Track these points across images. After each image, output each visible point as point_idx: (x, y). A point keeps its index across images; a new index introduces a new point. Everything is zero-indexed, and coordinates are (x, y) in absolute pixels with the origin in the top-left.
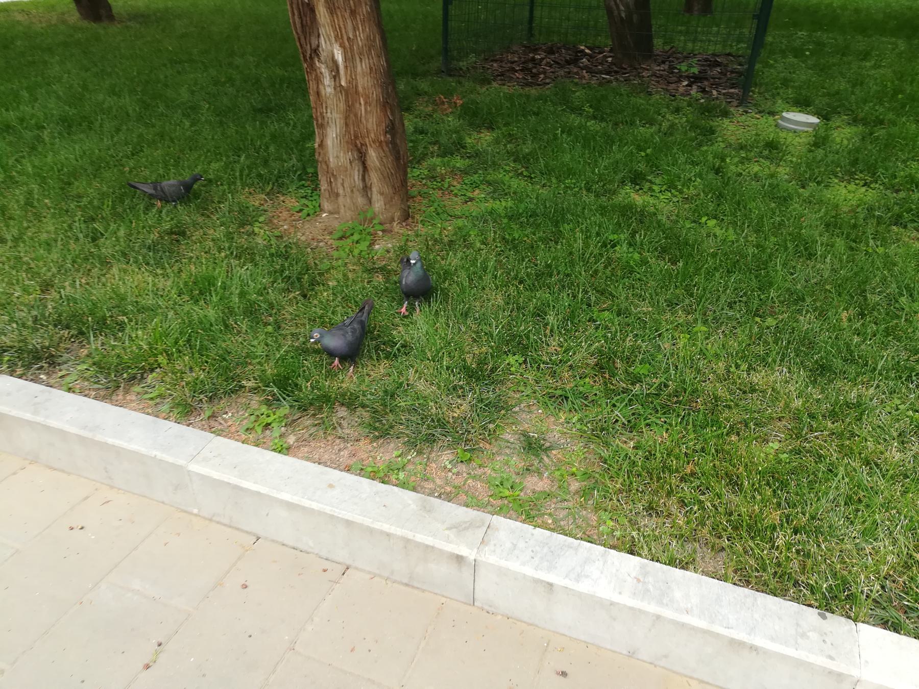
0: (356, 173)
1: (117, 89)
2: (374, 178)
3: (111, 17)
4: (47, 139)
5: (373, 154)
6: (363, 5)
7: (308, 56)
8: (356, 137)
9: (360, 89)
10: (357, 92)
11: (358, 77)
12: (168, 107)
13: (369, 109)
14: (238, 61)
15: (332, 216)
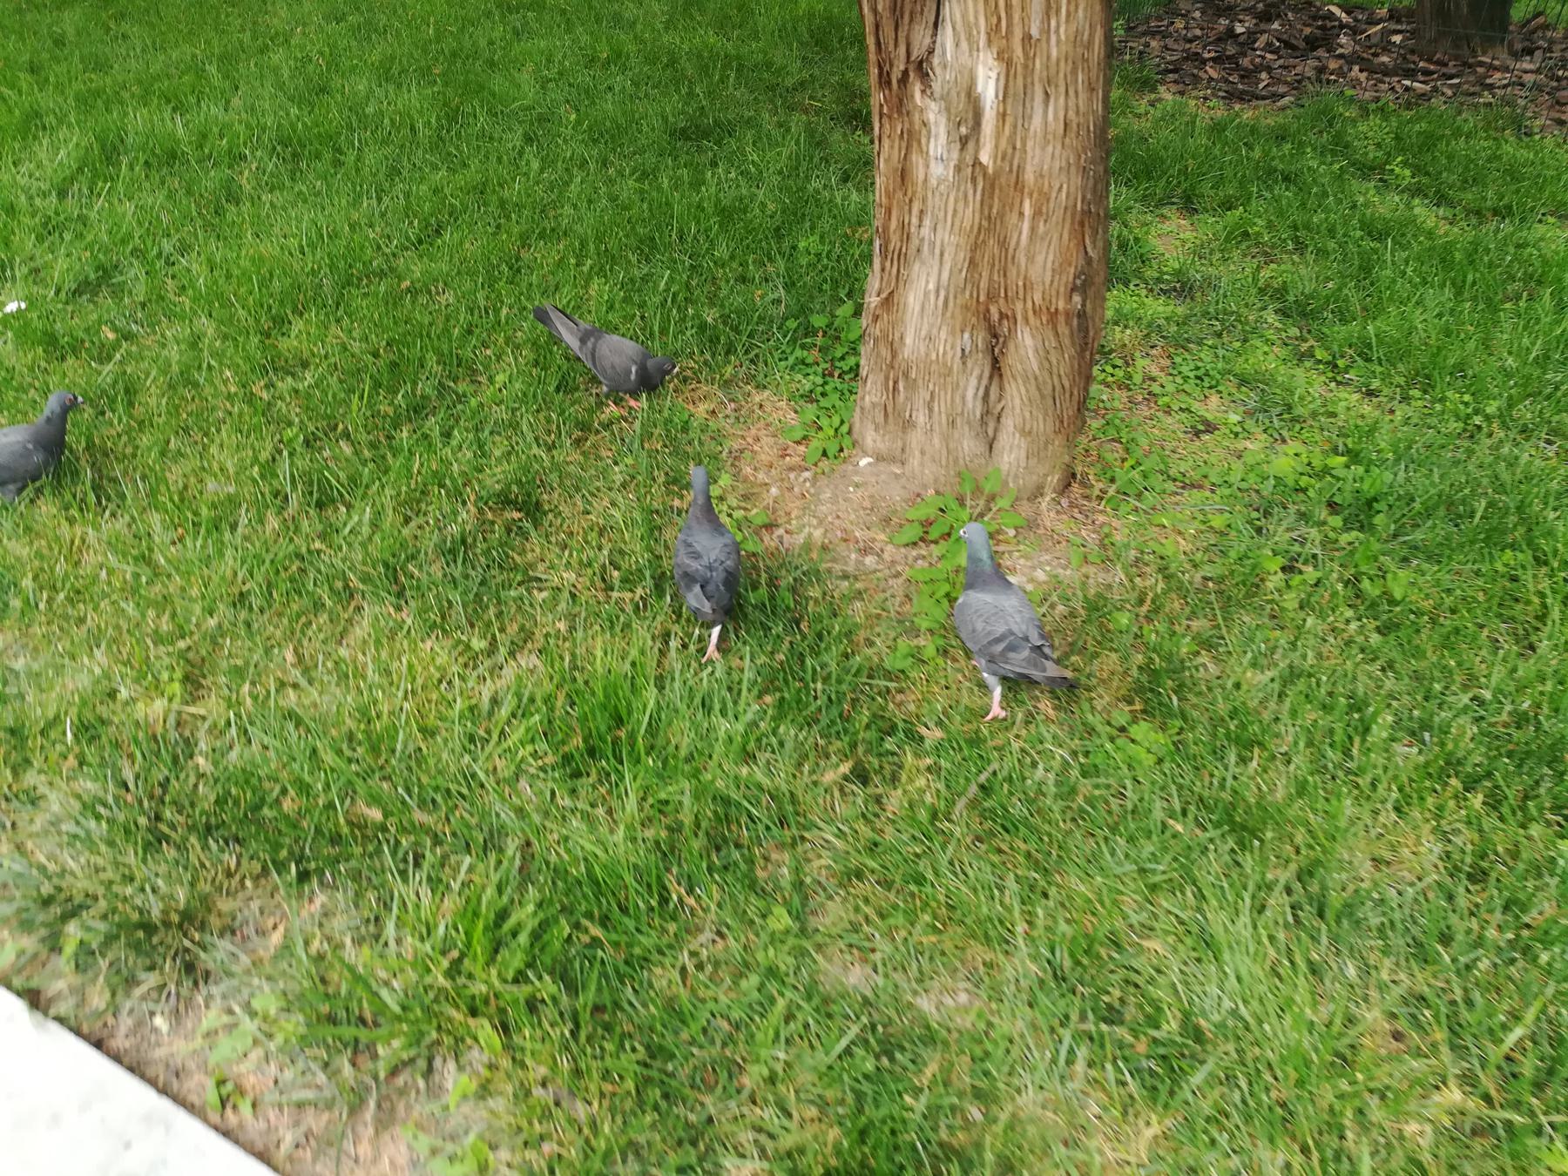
0: (973, 382)
1: (395, 71)
2: (1016, 396)
4: (247, 188)
5: (1029, 341)
7: (896, 75)
8: (992, 297)
9: (1029, 177)
10: (1019, 185)
11: (1030, 144)
12: (492, 113)
13: (1041, 228)
15: (882, 466)
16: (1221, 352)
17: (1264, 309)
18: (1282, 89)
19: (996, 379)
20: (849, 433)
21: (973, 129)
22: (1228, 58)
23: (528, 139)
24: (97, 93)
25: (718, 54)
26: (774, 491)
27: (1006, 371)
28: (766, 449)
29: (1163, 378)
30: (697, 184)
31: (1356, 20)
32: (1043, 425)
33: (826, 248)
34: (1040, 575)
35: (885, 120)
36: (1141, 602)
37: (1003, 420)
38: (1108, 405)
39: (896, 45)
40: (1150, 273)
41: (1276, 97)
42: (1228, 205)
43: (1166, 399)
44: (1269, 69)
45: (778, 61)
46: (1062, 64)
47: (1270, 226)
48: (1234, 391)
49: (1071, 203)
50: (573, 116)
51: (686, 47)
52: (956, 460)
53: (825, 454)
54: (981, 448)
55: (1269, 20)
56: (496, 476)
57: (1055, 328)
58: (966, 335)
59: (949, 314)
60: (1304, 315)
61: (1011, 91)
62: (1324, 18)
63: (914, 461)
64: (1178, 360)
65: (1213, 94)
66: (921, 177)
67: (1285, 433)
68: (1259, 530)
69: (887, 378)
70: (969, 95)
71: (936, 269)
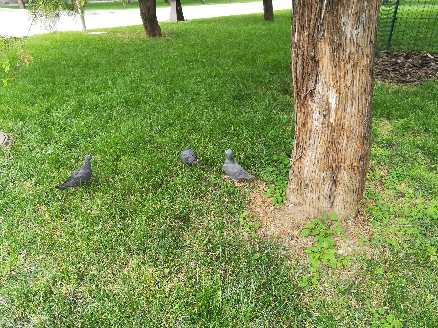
0: (327, 186)
1: (157, 81)
2: (341, 191)
3: (160, 35)
5: (345, 175)
6: (365, 58)
9: (346, 127)
10: (343, 129)
11: (346, 117)
12: (183, 92)
14: (222, 61)
15: (296, 207)
16: (404, 168)
17: (417, 153)
18: (415, 79)
19: (334, 185)
20: (285, 195)
21: (328, 112)
22: (397, 70)
23: (192, 100)
24: (80, 90)
25: (246, 73)
26: (261, 215)
27: (338, 184)
28: (259, 201)
29: (385, 177)
30: (239, 113)
31: (435, 57)
32: (350, 199)
33: (277, 133)
34: (350, 249)
35: (299, 108)
36: (386, 263)
37: (336, 197)
38: (368, 186)
39: (303, 87)
40: (379, 140)
41: (413, 82)
42: (401, 117)
43: (387, 184)
44: (410, 73)
45: (263, 74)
46: (357, 93)
47: (416, 124)
48: (410, 182)
49: (360, 134)
50: (205, 93)
51: (237, 71)
52: (321, 208)
53: (277, 202)
54: (329, 205)
55: (408, 58)
56: (176, 210)
57: (354, 171)
58: (325, 172)
59: (319, 166)
60: (431, 154)
61: (341, 102)
62: (425, 57)
63: (307, 208)
64: (390, 171)
65: (393, 81)
66: (310, 125)
67: (429, 197)
68: (425, 235)
69: (298, 181)
70: (327, 103)
71: (315, 152)
